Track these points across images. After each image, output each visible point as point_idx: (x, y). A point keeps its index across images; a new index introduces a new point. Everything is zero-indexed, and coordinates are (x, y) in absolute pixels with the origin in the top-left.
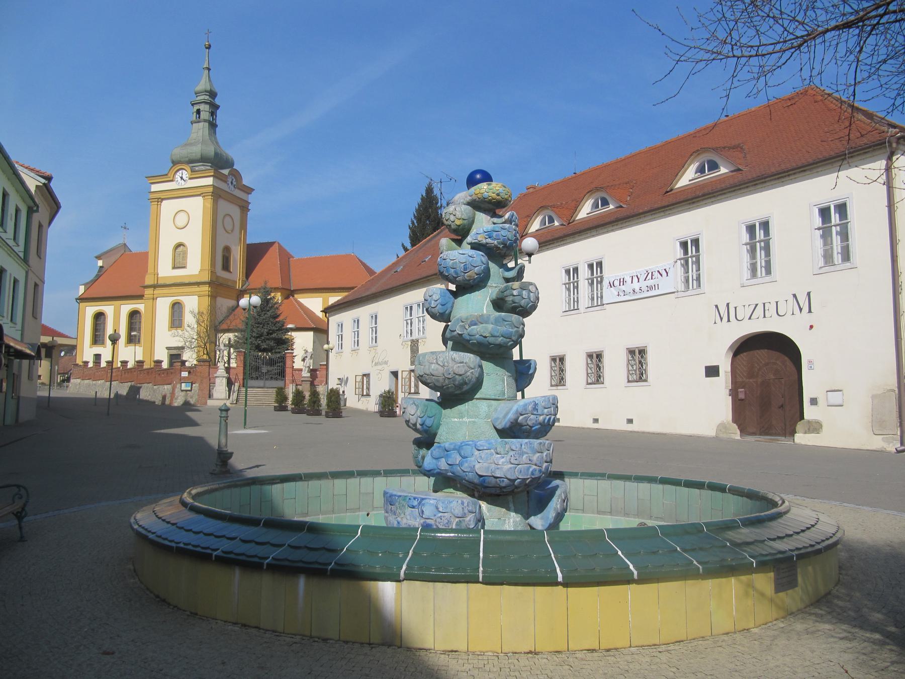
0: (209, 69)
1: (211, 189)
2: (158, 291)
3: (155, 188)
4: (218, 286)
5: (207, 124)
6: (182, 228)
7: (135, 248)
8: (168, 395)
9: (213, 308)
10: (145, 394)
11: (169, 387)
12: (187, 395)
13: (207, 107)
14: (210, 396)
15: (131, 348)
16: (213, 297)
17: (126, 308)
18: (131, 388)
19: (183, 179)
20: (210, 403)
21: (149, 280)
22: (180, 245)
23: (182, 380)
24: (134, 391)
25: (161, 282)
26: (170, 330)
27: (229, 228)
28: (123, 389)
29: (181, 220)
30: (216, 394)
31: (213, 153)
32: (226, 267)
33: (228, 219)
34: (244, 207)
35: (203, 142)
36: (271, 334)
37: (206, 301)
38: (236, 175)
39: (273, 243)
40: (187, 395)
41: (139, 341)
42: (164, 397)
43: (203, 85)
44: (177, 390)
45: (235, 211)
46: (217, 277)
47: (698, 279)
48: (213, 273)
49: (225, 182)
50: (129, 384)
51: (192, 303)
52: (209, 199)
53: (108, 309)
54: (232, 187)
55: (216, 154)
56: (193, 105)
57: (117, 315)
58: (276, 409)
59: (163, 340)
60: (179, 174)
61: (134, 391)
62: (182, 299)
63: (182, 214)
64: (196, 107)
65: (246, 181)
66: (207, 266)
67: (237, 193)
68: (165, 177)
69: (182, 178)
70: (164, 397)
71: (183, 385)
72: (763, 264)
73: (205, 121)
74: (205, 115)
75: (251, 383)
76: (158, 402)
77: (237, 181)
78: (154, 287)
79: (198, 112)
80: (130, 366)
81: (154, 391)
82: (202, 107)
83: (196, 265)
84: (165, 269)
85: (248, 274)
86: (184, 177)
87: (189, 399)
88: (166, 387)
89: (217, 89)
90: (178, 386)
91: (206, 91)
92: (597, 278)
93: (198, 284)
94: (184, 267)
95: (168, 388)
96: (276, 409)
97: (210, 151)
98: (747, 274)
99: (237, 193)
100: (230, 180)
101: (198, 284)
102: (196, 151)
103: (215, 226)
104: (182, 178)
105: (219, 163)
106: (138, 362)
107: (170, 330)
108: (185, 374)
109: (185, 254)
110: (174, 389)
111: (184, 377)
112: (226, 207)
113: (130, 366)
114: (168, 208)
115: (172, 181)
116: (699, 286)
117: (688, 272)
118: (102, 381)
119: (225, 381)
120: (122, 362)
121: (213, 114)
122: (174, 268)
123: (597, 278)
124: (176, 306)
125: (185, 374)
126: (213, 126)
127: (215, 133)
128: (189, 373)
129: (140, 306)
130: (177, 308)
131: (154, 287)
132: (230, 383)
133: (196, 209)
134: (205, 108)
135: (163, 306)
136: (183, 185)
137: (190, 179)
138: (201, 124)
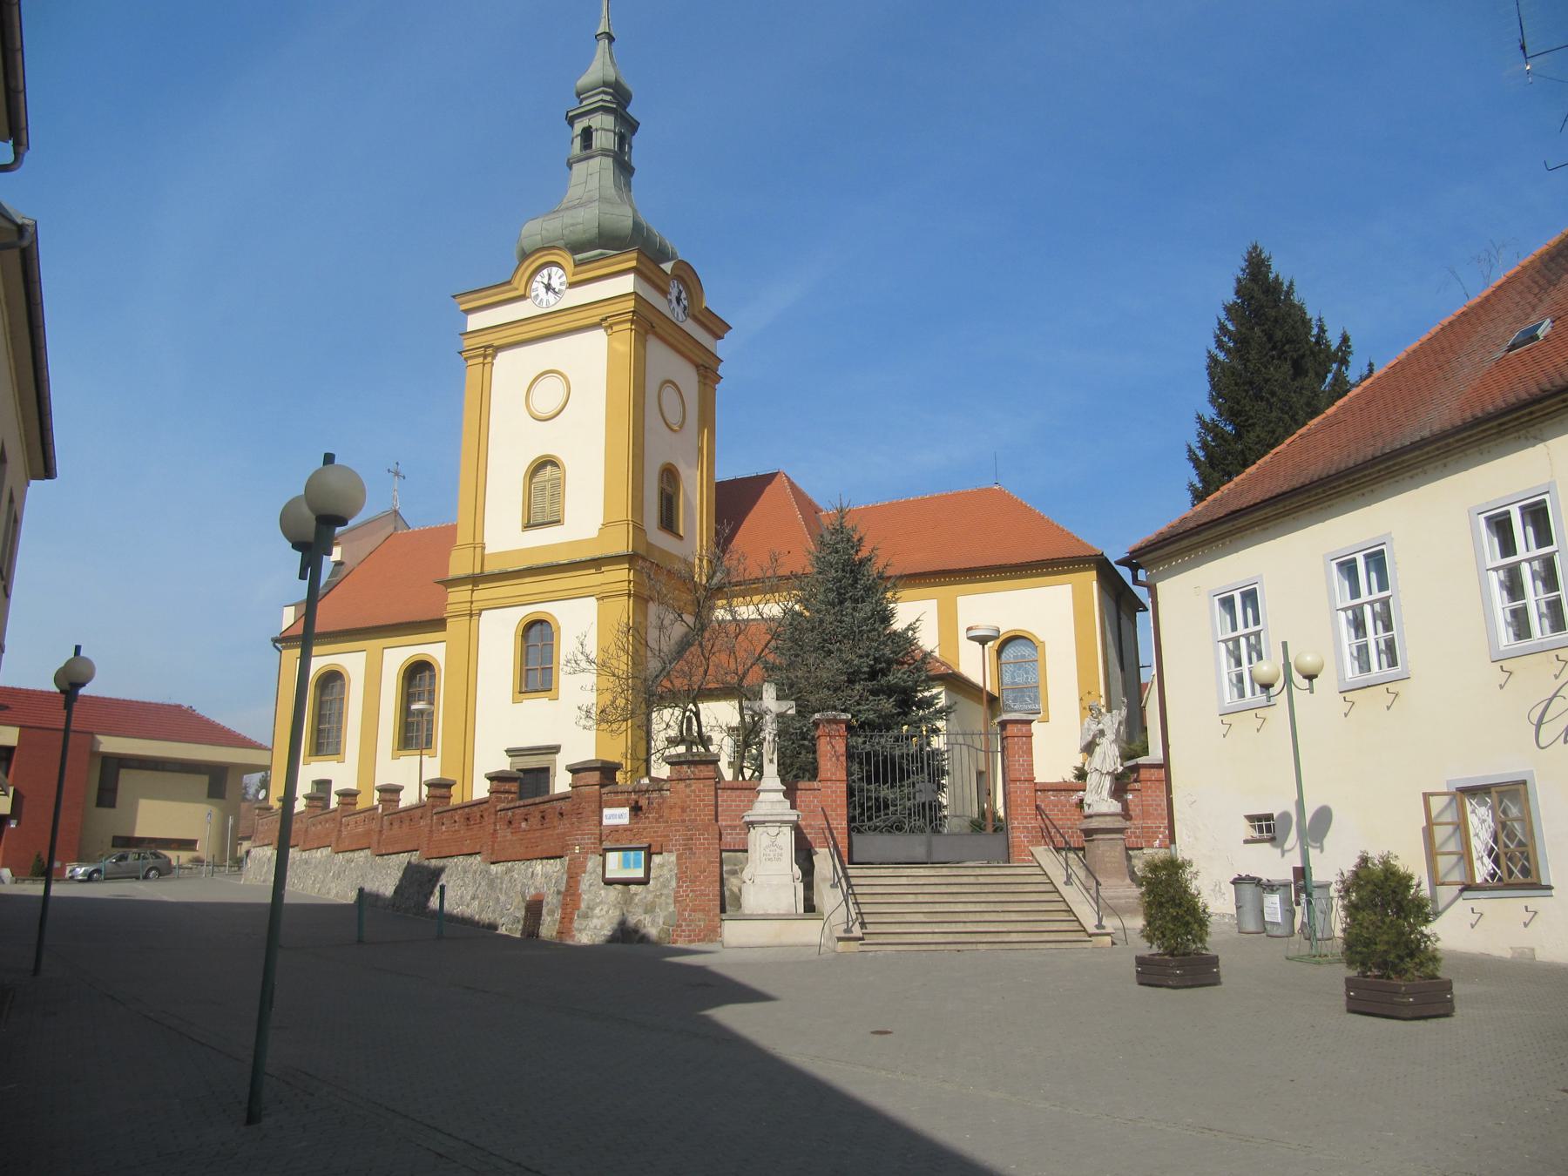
0: (611, 39)
1: (630, 305)
2: (484, 593)
3: (475, 322)
4: (649, 572)
5: (609, 162)
6: (551, 416)
7: (419, 519)
8: (551, 900)
9: (637, 631)
10: (472, 890)
11: (554, 868)
12: (628, 900)
13: (608, 121)
14: (727, 903)
15: (410, 761)
16: (640, 598)
17: (397, 656)
18: (410, 871)
19: (556, 288)
20: (734, 932)
21: (460, 564)
22: (544, 463)
23: (608, 842)
24: (421, 880)
25: (490, 568)
26: (530, 698)
27: (674, 419)
28: (385, 879)
29: (548, 396)
30: (753, 899)
31: (630, 223)
32: (668, 522)
33: (669, 393)
34: (708, 370)
35: (602, 199)
36: (884, 672)
37: (622, 608)
38: (687, 277)
39: (773, 476)
40: (628, 900)
41: (429, 743)
42: (534, 909)
43: (599, 68)
44: (588, 882)
45: (687, 377)
46: (649, 545)
47: (1390, 646)
48: (638, 529)
49: (665, 293)
50: (404, 858)
51: (583, 623)
52: (625, 338)
53: (351, 661)
54: (679, 310)
55: (637, 226)
56: (571, 121)
57: (370, 672)
58: (1150, 973)
59: (501, 725)
60: (542, 277)
61: (421, 880)
62: (555, 610)
63: (551, 382)
64: (579, 126)
65: (712, 300)
66: (623, 511)
67: (690, 327)
68: (503, 290)
69: (548, 287)
70: (534, 909)
71: (613, 858)
72: (1382, 646)
73: (604, 152)
74: (604, 139)
75: (869, 844)
76: (510, 924)
77: (690, 297)
78: (475, 580)
79: (587, 134)
80: (408, 799)
81: (491, 884)
82: (597, 121)
83: (590, 513)
84: (504, 533)
85: (723, 540)
86: (555, 283)
87: (636, 917)
88: (539, 867)
89: (629, 84)
90: (593, 862)
91: (605, 84)
92: (1247, 637)
93: (597, 563)
94: (558, 522)
95: (544, 875)
96: (1150, 973)
97: (622, 217)
98: (1505, 636)
99: (690, 327)
100: (674, 292)
101: (597, 563)
102: (585, 219)
103: (643, 408)
104: (548, 287)
105: (646, 251)
106: (430, 785)
107: (530, 698)
108: (616, 816)
109: (558, 487)
110: (573, 877)
111: (615, 829)
112: (665, 363)
113: (408, 799)
114: (511, 369)
115: (523, 297)
116: (1393, 662)
117: (1239, 663)
118: (327, 851)
119: (786, 838)
120: (382, 790)
121: (622, 140)
122: (528, 526)
123: (1247, 637)
124: (535, 630)
125: (616, 816)
126: (624, 168)
127: (628, 185)
128: (636, 809)
129: (434, 650)
130: (536, 636)
131: (475, 580)
132: (804, 855)
133: (591, 365)
134: (603, 123)
135: (498, 633)
136: (550, 302)
137: (572, 285)
138: (595, 163)
